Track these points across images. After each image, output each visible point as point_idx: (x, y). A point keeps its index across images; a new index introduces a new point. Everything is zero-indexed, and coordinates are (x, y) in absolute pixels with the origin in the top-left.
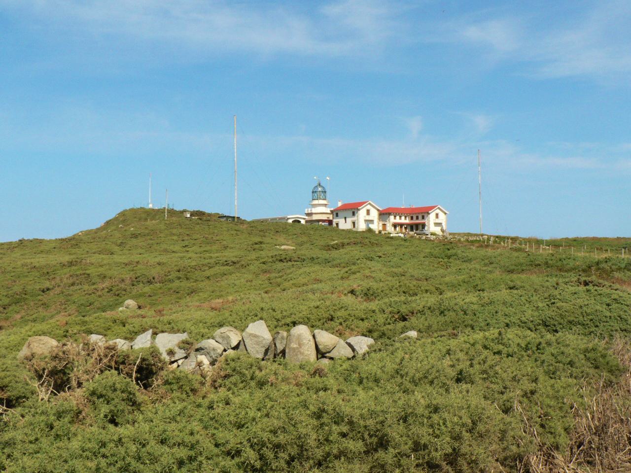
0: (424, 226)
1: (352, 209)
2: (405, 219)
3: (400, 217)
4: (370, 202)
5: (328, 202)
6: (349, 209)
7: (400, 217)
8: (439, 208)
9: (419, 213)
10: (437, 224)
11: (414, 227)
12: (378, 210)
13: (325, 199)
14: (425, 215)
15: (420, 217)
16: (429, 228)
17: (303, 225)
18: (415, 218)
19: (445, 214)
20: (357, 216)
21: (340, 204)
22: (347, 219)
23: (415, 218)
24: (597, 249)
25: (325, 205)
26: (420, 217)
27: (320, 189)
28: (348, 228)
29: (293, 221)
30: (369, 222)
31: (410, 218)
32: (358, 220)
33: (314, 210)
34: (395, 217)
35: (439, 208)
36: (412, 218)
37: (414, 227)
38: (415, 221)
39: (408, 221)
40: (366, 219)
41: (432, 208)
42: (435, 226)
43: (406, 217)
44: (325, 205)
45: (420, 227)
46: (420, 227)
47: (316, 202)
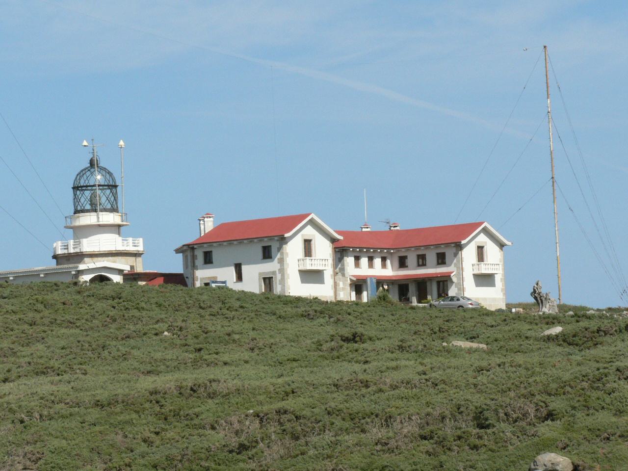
0: (443, 283)
1: (267, 241)
2: (384, 266)
3: (371, 259)
4: (312, 216)
5: (124, 216)
6: (251, 240)
7: (371, 259)
8: (312, 223)
9: (408, 249)
10: (484, 279)
11: (412, 289)
12: (333, 240)
13: (114, 210)
14: (274, 246)
15: (431, 257)
16: (461, 289)
17: (118, 283)
18: (412, 260)
19: (501, 246)
20: (281, 261)
21: (209, 225)
22: (245, 269)
23: (412, 260)
24: (106, 381)
25: (117, 228)
26: (431, 257)
27: (99, 177)
28: (252, 291)
29: (92, 280)
30: (312, 276)
31: (397, 263)
32: (282, 271)
33: (89, 245)
34: (357, 259)
35: (312, 223)
36: (402, 263)
37: (412, 289)
38: (413, 271)
39: (390, 271)
40: (309, 272)
41: (292, 221)
42: (304, 281)
43: (384, 259)
44: (117, 228)
45: (433, 289)
46: (433, 289)
47: (89, 219)
